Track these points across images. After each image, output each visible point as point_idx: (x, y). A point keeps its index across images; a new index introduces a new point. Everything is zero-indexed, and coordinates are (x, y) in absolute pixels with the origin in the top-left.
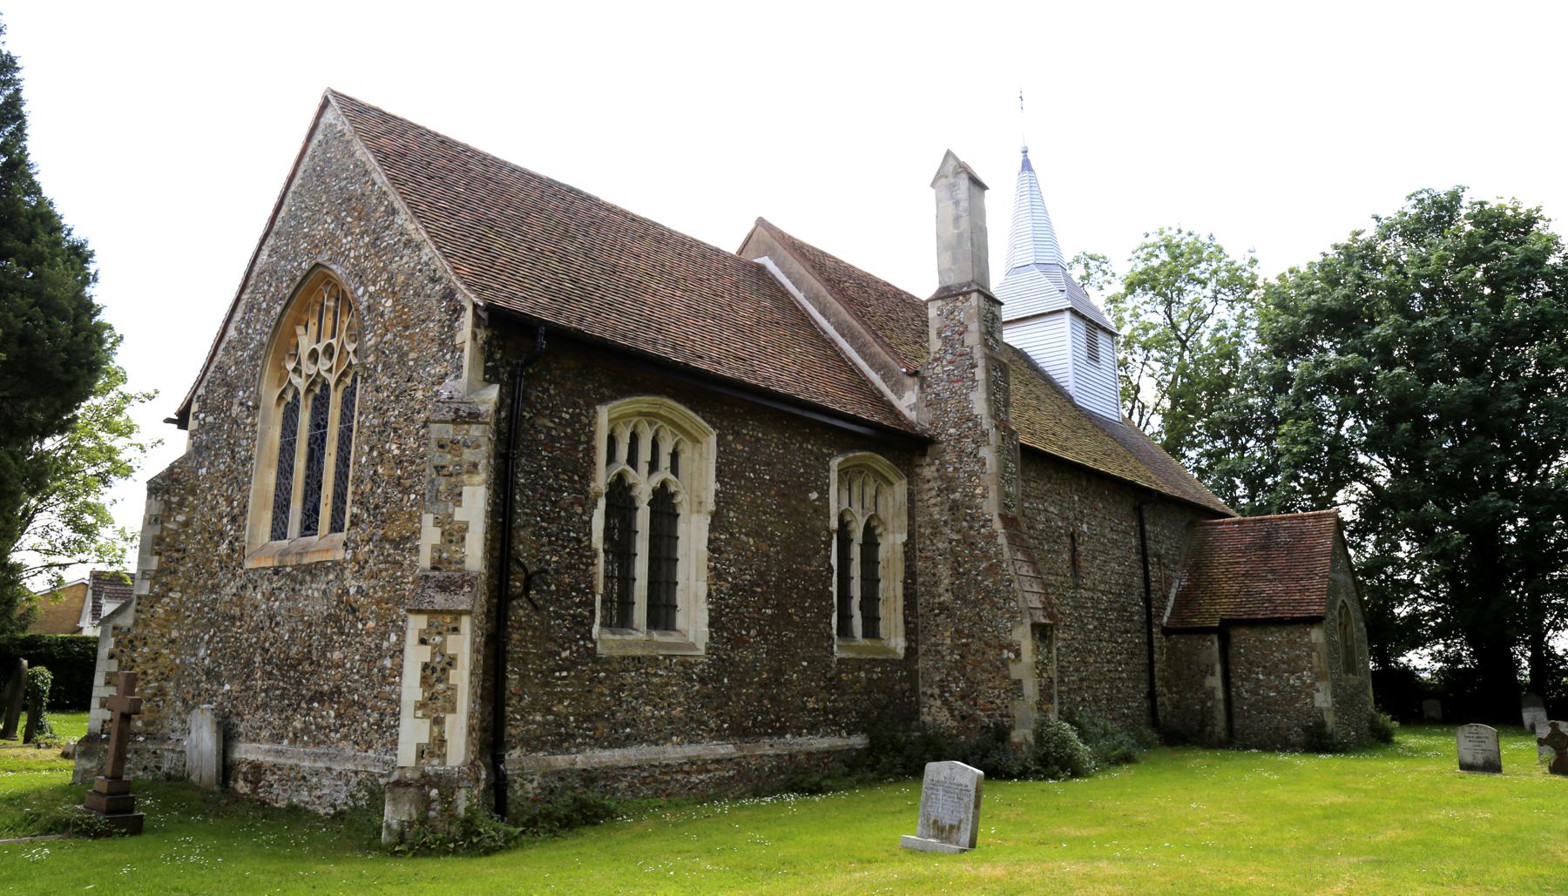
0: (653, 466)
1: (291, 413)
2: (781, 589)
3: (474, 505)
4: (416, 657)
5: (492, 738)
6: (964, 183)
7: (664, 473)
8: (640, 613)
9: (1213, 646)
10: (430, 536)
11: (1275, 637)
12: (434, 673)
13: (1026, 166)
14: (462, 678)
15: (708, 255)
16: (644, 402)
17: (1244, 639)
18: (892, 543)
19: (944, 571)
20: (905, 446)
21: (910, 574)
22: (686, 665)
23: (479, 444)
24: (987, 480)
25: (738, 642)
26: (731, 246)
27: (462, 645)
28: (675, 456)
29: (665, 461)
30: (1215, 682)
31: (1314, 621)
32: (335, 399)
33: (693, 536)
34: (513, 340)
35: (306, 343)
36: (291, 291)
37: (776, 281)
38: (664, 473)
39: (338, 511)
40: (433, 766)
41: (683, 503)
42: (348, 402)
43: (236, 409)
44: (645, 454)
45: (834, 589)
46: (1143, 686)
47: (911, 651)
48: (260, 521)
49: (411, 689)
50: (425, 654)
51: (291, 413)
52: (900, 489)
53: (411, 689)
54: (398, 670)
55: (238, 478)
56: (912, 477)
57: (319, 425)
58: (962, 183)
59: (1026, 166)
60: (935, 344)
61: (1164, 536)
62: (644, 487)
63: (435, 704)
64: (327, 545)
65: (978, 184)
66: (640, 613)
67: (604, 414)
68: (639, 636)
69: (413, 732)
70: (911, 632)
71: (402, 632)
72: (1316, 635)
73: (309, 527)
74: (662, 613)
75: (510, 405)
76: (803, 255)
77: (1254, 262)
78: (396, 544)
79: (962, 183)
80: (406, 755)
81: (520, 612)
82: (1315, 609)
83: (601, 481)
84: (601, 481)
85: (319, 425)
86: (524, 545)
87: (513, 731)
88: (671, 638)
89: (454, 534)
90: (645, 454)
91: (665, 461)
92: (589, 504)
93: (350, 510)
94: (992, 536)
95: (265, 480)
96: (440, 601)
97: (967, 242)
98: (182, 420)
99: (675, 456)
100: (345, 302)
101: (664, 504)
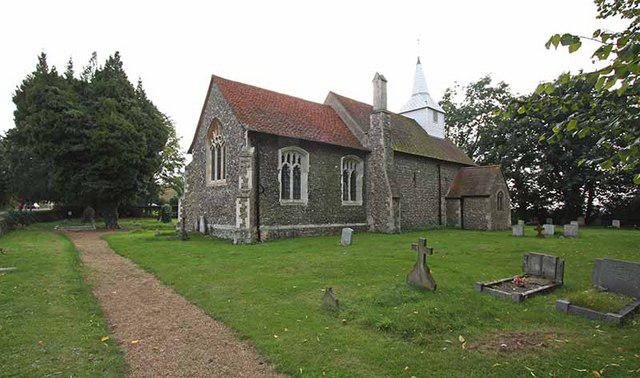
0: (294, 162)
1: (213, 153)
2: (324, 192)
3: (250, 174)
4: (238, 206)
5: (257, 222)
6: (380, 81)
7: (286, 162)
9: (459, 202)
10: (241, 181)
11: (477, 200)
12: (243, 210)
13: (419, 62)
15: (319, 105)
16: (291, 148)
17: (467, 200)
18: (359, 177)
19: (373, 184)
20: (364, 154)
22: (303, 208)
23: (250, 162)
24: (382, 160)
25: (315, 202)
26: (322, 102)
28: (299, 160)
29: (297, 161)
30: (459, 212)
31: (488, 196)
33: (304, 178)
34: (256, 137)
36: (208, 124)
37: (341, 109)
38: (286, 162)
40: (243, 228)
41: (302, 169)
44: (291, 159)
46: (437, 213)
49: (238, 213)
51: (213, 153)
52: (362, 164)
53: (238, 213)
55: (203, 167)
57: (219, 154)
58: (381, 80)
59: (419, 62)
61: (446, 172)
62: (291, 167)
63: (243, 216)
64: (223, 182)
65: (384, 81)
68: (350, 202)
69: (239, 221)
72: (487, 200)
73: (219, 178)
74: (297, 195)
75: (257, 151)
77: (581, 71)
79: (381, 80)
80: (238, 226)
81: (262, 196)
82: (488, 193)
83: (280, 167)
84: (280, 167)
85: (219, 154)
86: (262, 182)
87: (262, 221)
88: (300, 201)
89: (246, 181)
90: (291, 159)
91: (297, 161)
94: (384, 176)
96: (243, 195)
97: (382, 96)
98: (190, 152)
99: (299, 160)
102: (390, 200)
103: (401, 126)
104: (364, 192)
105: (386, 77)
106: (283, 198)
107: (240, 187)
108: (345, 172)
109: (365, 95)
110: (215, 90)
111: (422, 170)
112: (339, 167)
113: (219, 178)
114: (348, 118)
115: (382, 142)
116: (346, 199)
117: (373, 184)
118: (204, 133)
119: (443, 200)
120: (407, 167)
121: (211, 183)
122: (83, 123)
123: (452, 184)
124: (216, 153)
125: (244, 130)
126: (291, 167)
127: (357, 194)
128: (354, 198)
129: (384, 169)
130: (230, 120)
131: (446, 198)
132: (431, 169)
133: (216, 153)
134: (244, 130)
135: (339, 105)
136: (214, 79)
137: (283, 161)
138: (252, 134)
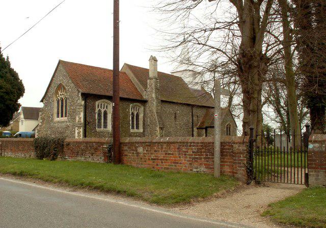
3: (82, 115)
7: (100, 108)
8: (135, 127)
9: (204, 130)
10: (77, 119)
12: (79, 133)
14: (81, 133)
16: (102, 100)
17: (208, 129)
18: (141, 116)
19: (149, 120)
20: (144, 102)
21: (144, 120)
22: (108, 133)
23: (82, 109)
24: (153, 105)
27: (81, 130)
29: (105, 107)
32: (64, 101)
34: (85, 96)
35: (60, 93)
36: (54, 87)
38: (100, 108)
39: (66, 113)
42: (66, 101)
43: (50, 101)
44: (103, 106)
45: (131, 123)
47: (144, 131)
48: (55, 115)
50: (78, 131)
52: (142, 108)
54: (75, 133)
56: (144, 106)
57: (62, 104)
60: (148, 86)
61: (197, 112)
62: (103, 111)
64: (65, 119)
65: (156, 60)
66: (135, 127)
67: (97, 103)
68: (135, 130)
70: (144, 128)
71: (75, 129)
73: (62, 116)
74: (105, 126)
75: (85, 103)
76: (30, 175)
78: (73, 119)
81: (88, 126)
85: (62, 104)
86: (88, 119)
89: (80, 118)
90: (103, 106)
91: (100, 107)
92: (95, 114)
93: (67, 115)
95: (56, 110)
100: (65, 89)
101: (105, 113)
102: (158, 129)
103: (168, 82)
104: (144, 124)
105: (158, 58)
106: (98, 127)
107: (77, 121)
108: (133, 114)
109: (145, 64)
110: (61, 68)
111: (179, 110)
112: (129, 110)
113: (62, 116)
114: (135, 80)
115: (154, 95)
116: (133, 128)
117: (149, 120)
118: (52, 90)
119: (195, 129)
120: (169, 109)
121: (56, 119)
122: (247, 152)
123: (201, 119)
124: (60, 103)
125: (79, 92)
126: (103, 111)
127: (108, 124)
128: (138, 128)
129: (155, 111)
130: (66, 81)
131: (197, 128)
132: (187, 110)
133: (60, 103)
134: (79, 92)
135: (130, 72)
136: (60, 62)
137: (98, 107)
138: (83, 94)
